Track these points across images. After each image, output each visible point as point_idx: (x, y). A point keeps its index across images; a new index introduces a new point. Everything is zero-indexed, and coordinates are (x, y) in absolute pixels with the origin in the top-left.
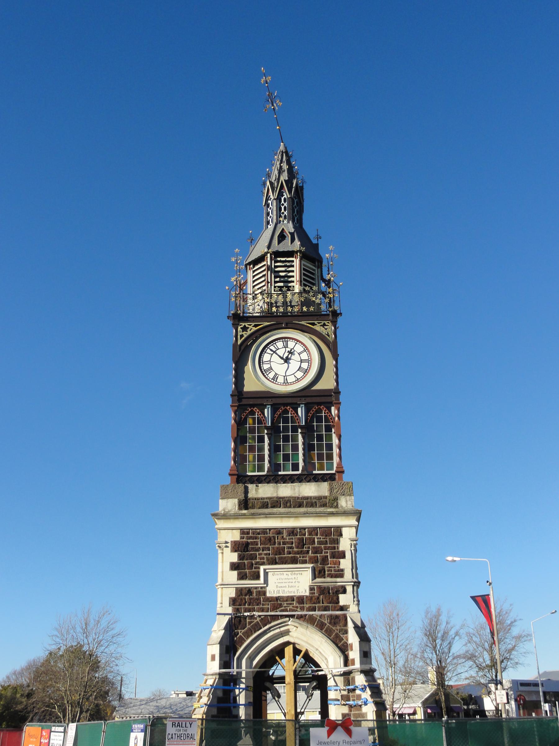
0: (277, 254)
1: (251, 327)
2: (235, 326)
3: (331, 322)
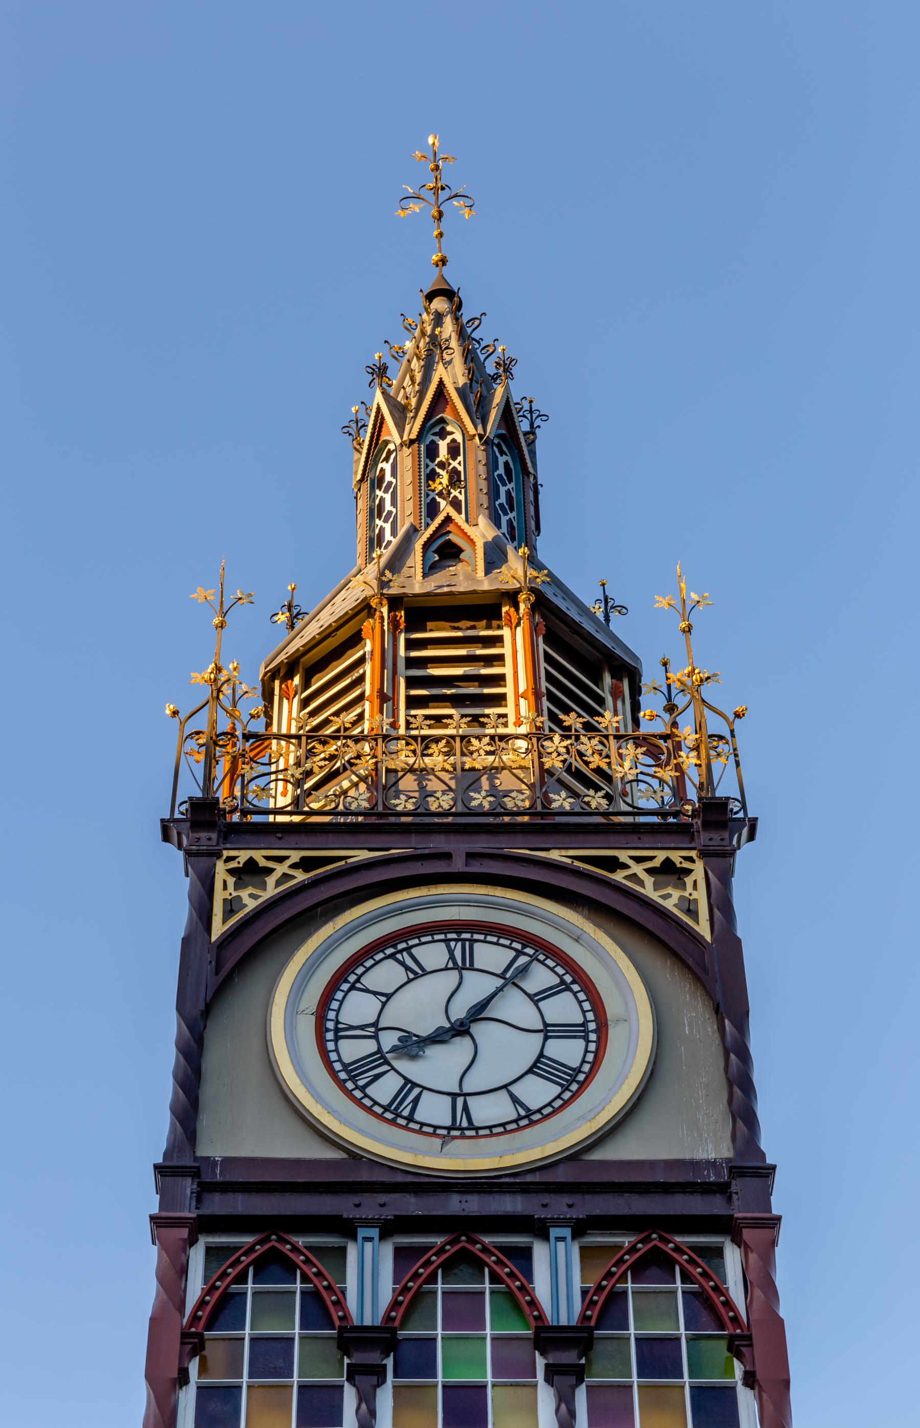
0: (417, 613)
1: (281, 869)
2: (200, 861)
3: (703, 854)
